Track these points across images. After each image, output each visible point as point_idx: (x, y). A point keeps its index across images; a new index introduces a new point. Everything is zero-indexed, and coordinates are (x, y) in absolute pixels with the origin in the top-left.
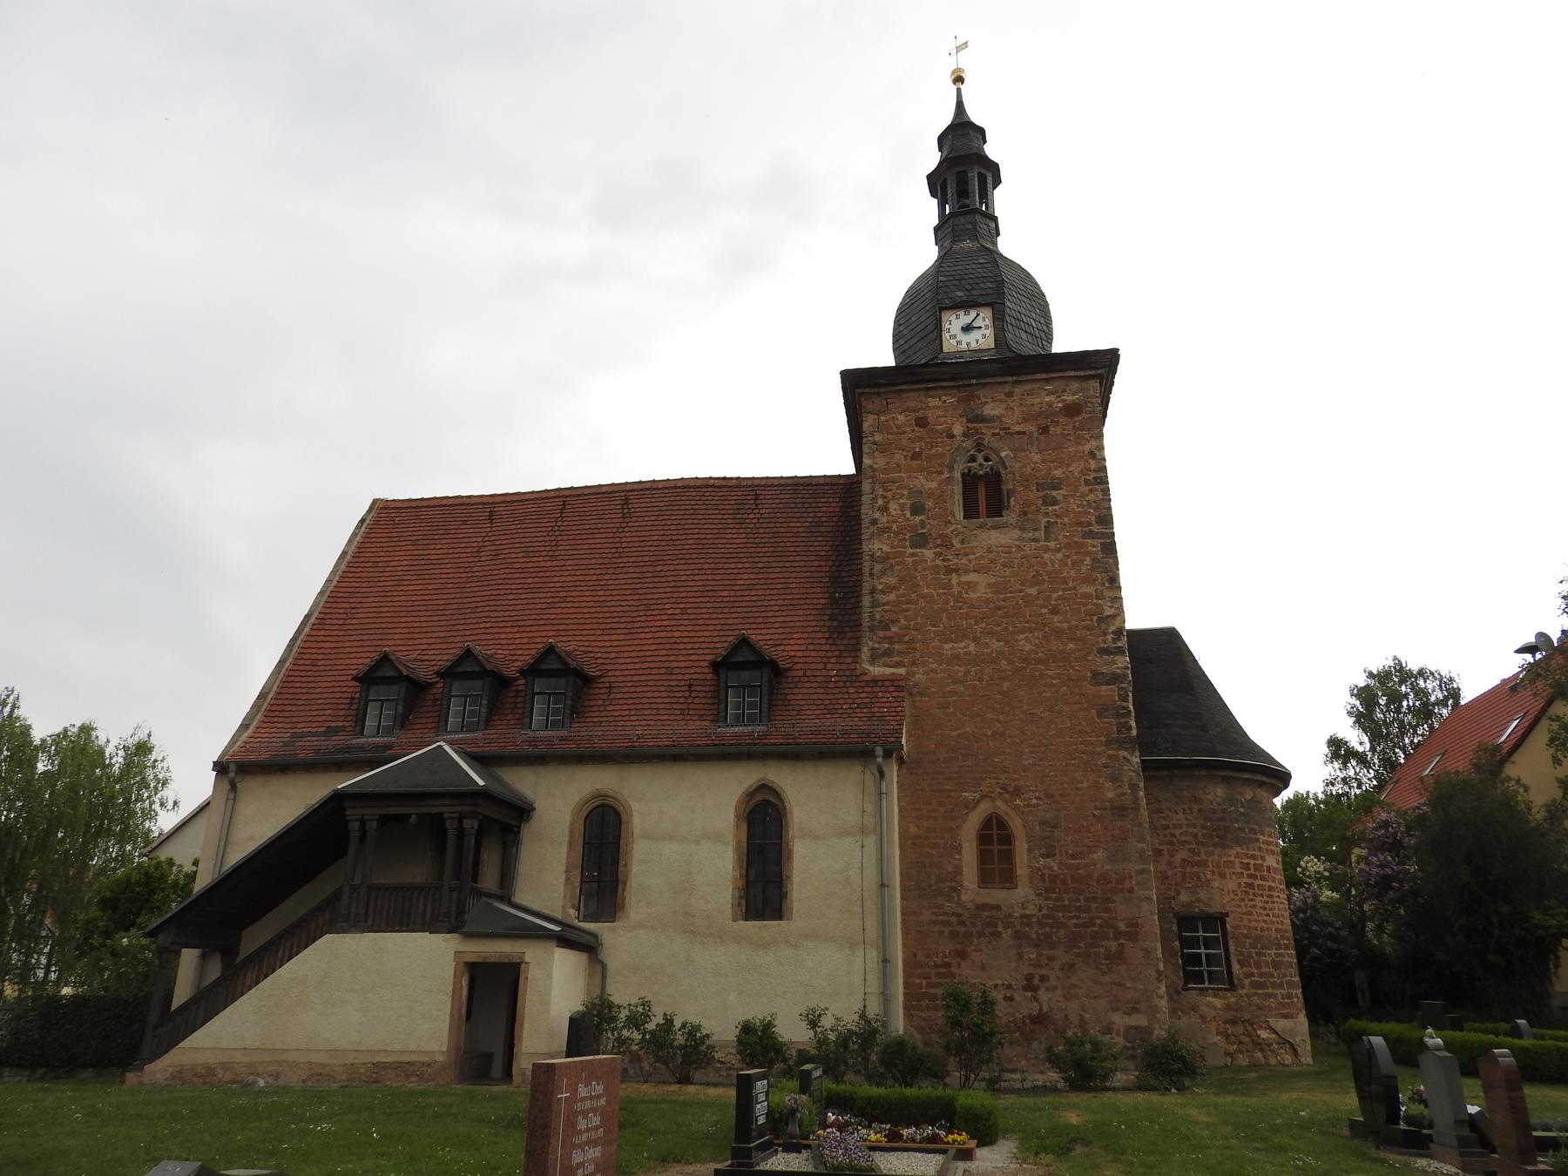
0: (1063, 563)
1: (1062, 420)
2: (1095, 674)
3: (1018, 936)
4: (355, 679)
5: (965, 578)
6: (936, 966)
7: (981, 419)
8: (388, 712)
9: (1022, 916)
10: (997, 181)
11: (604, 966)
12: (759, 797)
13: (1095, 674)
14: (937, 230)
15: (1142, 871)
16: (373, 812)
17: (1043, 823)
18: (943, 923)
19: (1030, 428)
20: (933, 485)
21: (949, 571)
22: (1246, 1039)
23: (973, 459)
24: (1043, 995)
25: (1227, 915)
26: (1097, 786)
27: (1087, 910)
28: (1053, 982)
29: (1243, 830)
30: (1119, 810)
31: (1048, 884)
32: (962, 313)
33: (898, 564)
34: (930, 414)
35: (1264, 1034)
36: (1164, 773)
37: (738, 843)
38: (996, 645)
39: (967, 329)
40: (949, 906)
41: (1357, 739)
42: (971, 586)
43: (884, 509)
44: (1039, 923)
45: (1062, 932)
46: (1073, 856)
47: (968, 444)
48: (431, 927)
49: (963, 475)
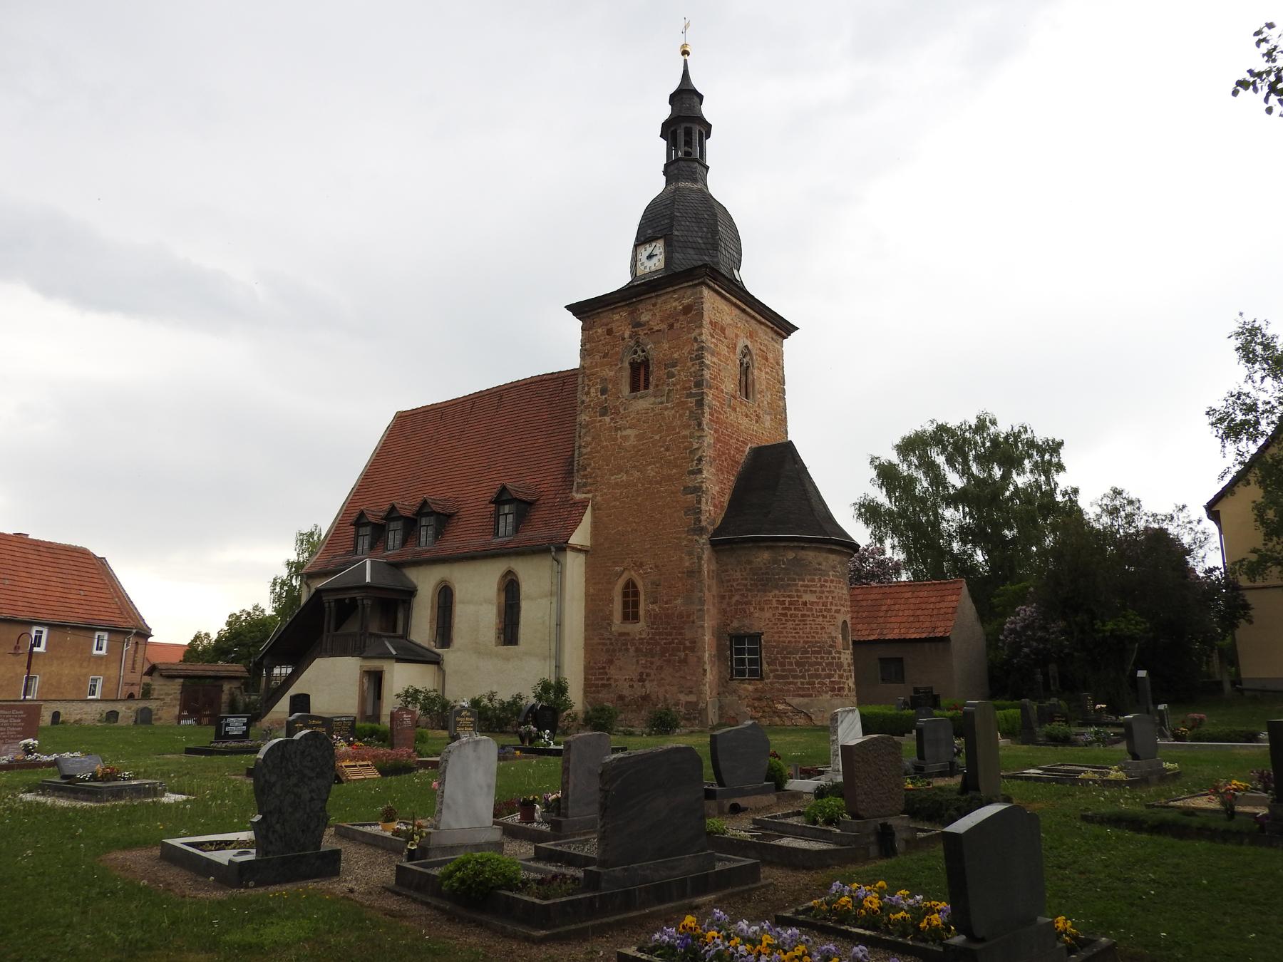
0: (674, 417)
2: (685, 488)
3: (637, 650)
4: (491, 502)
5: (625, 433)
7: (639, 325)
8: (430, 532)
10: (708, 136)
11: (444, 672)
13: (685, 488)
16: (333, 597)
20: (612, 374)
21: (617, 429)
22: (767, 709)
23: (636, 352)
26: (681, 559)
28: (653, 677)
29: (783, 580)
31: (654, 619)
34: (614, 326)
35: (780, 707)
38: (637, 474)
39: (650, 257)
40: (606, 634)
42: (626, 438)
43: (588, 393)
47: (632, 343)
48: (344, 653)
49: (631, 364)
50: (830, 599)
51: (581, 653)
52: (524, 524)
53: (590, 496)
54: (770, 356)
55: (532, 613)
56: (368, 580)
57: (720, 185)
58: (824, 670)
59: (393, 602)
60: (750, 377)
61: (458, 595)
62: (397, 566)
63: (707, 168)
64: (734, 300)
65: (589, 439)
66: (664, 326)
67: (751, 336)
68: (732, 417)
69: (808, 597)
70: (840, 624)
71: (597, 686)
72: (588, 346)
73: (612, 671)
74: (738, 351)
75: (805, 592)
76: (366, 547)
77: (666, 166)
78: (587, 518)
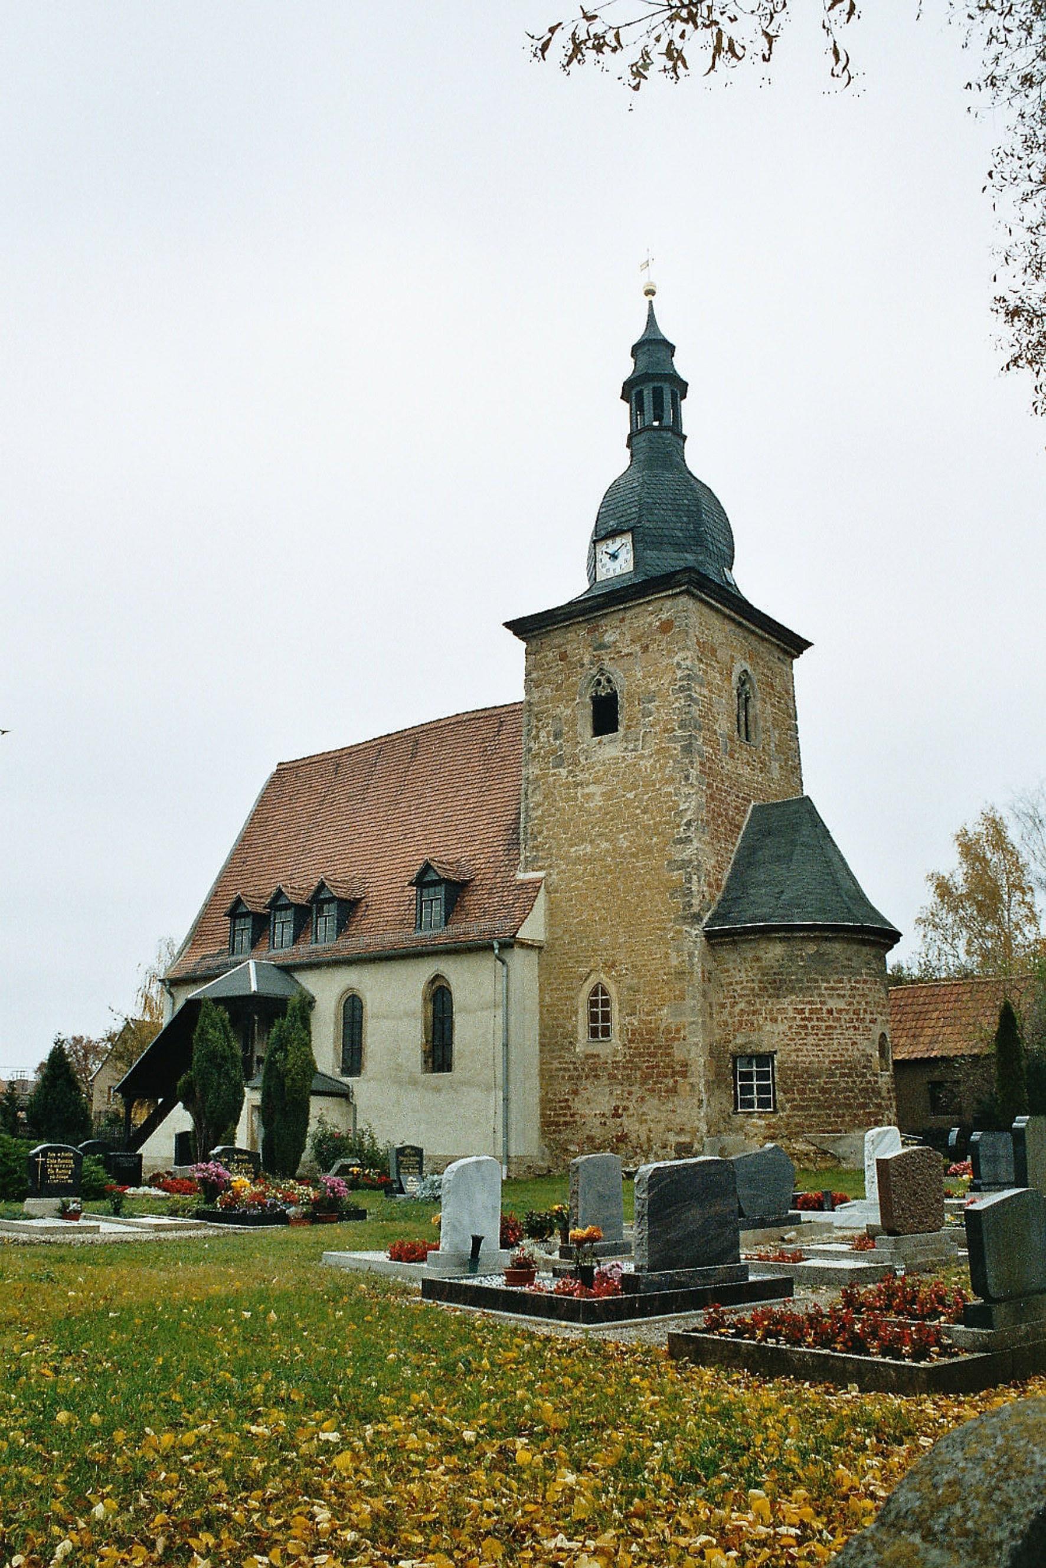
0: (653, 766)
1: (658, 637)
4: (411, 884)
5: (587, 790)
7: (602, 646)
12: (437, 984)
15: (693, 1023)
17: (630, 988)
18: (565, 1069)
19: (636, 648)
20: (569, 711)
21: (577, 785)
25: (775, 1052)
27: (653, 1055)
28: (631, 1112)
30: (680, 974)
32: (610, 542)
38: (605, 845)
41: (959, 881)
42: (589, 797)
43: (536, 738)
45: (638, 1074)
46: (648, 1014)
53: (541, 874)
55: (469, 1031)
57: (701, 459)
61: (369, 1009)
62: (287, 970)
63: (684, 438)
64: (727, 611)
66: (636, 648)
69: (832, 1004)
71: (557, 1124)
72: (534, 675)
73: (577, 1105)
75: (831, 996)
76: (246, 943)
77: (630, 438)
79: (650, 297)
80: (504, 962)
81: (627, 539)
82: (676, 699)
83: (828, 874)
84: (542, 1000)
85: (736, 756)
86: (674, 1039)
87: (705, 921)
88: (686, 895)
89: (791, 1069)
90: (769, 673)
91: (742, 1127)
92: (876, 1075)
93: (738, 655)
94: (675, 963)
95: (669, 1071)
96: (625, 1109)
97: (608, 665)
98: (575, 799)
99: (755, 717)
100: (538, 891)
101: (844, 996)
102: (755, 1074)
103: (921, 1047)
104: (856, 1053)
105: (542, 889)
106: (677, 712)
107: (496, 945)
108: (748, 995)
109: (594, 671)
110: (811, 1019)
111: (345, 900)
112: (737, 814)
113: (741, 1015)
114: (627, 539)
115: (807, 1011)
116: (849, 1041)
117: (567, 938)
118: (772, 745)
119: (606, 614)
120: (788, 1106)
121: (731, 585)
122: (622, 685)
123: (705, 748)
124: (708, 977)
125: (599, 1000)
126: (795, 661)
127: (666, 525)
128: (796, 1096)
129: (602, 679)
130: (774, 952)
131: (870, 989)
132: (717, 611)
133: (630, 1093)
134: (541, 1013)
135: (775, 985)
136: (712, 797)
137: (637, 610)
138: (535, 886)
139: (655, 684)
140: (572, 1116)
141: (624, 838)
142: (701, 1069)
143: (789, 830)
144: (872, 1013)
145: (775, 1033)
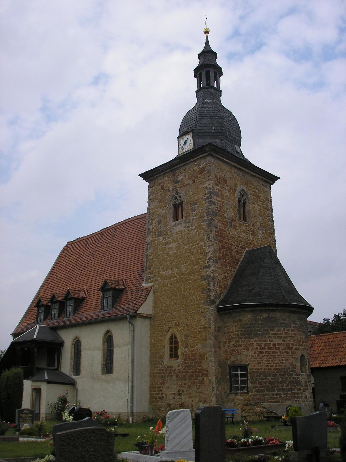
6: (157, 388)
7: (177, 182)
9: (178, 369)
12: (108, 334)
14: (197, 92)
17: (185, 335)
20: (164, 211)
21: (166, 244)
24: (183, 397)
25: (248, 365)
26: (200, 320)
27: (194, 366)
28: (185, 393)
29: (260, 331)
30: (205, 328)
33: (154, 244)
36: (226, 312)
37: (104, 350)
38: (176, 270)
39: (185, 143)
42: (171, 249)
43: (151, 224)
44: (182, 372)
45: (188, 374)
46: (192, 347)
50: (292, 342)
51: (147, 378)
52: (117, 301)
53: (151, 284)
54: (262, 195)
55: (121, 355)
56: (35, 337)
58: (287, 386)
59: (52, 349)
60: (247, 208)
62: (54, 329)
64: (232, 163)
65: (152, 251)
66: (190, 181)
67: (246, 184)
68: (232, 232)
69: (276, 341)
70: (299, 356)
73: (164, 389)
74: (237, 193)
75: (275, 337)
78: (150, 299)
79: (207, 34)
80: (132, 324)
81: (191, 134)
82: (205, 203)
83: (276, 280)
84: (151, 341)
85: (237, 228)
86: (202, 359)
87: (217, 303)
88: (208, 292)
89: (256, 372)
90: (257, 191)
91: (233, 400)
92: (298, 375)
93: (239, 183)
94: (203, 323)
95: (201, 373)
96: (183, 391)
97: (179, 190)
98: (165, 250)
99: (249, 210)
100: (149, 292)
101: (281, 337)
102: (239, 375)
103: (337, 361)
104: (288, 365)
105: (152, 290)
106: (205, 208)
107: (128, 317)
108: (236, 338)
109: (174, 193)
110: (265, 349)
111: (78, 299)
112: (237, 254)
113: (233, 347)
114: (191, 134)
115: (263, 345)
116: (284, 359)
117: (161, 313)
118: (258, 223)
119: (178, 168)
120: (254, 390)
121: (238, 153)
122: (184, 198)
123: (219, 224)
124: (218, 329)
125: (173, 341)
126: (271, 186)
127: (207, 128)
128: (258, 385)
129: (177, 196)
130: (248, 317)
131: (295, 334)
132: (224, 162)
133: (185, 384)
134: (151, 347)
135: (248, 333)
136: (223, 247)
137: (191, 165)
138: (148, 290)
139: (197, 196)
140: (162, 394)
141: (184, 266)
142: (214, 373)
143: (262, 261)
144: (296, 345)
145: (248, 356)
